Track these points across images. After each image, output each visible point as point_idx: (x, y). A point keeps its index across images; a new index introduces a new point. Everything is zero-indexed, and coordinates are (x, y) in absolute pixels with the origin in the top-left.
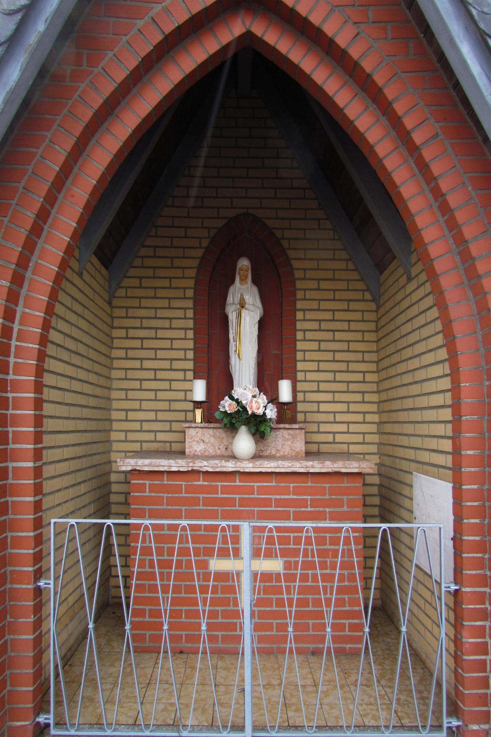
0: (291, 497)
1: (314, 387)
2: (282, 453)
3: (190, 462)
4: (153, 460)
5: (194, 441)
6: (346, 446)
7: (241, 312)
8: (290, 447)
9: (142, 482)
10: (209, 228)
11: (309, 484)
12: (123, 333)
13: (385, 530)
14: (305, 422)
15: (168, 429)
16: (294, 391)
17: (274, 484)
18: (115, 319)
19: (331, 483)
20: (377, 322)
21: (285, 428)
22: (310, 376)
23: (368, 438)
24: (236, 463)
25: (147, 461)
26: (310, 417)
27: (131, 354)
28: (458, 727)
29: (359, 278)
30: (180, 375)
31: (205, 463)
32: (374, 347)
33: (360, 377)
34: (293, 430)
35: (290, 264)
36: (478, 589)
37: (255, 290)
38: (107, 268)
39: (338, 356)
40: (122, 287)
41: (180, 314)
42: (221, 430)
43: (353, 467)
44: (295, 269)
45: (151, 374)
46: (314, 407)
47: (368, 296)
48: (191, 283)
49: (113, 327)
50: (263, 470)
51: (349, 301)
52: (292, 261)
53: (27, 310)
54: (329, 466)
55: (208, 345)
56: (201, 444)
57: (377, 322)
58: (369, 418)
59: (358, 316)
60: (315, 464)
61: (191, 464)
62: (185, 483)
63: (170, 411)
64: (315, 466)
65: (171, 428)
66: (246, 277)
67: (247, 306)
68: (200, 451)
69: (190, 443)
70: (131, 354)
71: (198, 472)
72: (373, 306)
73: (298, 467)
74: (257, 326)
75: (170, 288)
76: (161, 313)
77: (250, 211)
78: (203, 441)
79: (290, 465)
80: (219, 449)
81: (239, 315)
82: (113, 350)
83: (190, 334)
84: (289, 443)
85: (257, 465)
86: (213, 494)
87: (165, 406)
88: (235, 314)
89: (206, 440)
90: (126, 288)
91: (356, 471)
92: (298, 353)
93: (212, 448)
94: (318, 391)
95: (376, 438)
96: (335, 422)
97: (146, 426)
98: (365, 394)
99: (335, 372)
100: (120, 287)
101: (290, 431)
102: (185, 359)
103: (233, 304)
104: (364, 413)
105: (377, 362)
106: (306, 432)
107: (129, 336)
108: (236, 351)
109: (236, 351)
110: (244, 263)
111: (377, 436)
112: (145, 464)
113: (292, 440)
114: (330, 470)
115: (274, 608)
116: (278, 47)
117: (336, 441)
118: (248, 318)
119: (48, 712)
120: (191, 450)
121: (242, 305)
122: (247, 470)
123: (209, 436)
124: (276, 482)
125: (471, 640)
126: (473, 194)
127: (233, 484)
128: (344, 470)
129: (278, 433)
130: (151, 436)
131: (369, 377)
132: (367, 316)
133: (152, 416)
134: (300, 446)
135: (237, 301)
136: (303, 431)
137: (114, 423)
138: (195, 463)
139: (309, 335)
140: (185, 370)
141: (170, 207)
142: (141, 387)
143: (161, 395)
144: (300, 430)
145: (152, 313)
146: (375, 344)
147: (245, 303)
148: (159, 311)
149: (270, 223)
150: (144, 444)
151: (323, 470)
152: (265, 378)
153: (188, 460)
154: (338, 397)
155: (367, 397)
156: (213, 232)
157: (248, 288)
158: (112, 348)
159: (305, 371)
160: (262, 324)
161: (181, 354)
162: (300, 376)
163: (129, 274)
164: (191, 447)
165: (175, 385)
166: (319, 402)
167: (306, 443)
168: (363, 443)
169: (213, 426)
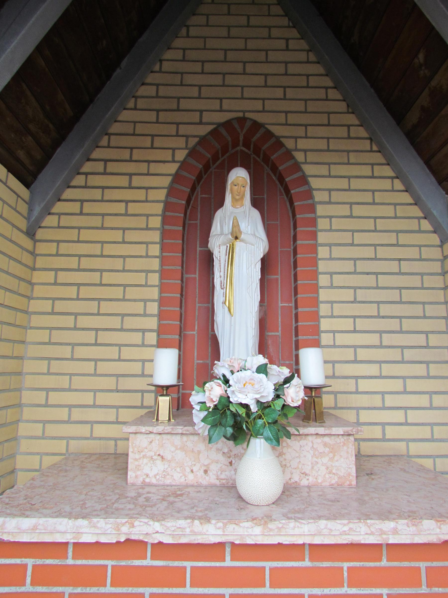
0: (345, 590)
1: (349, 354)
3: (124, 524)
4: (42, 521)
5: (144, 456)
6: (404, 444)
7: (233, 245)
8: (327, 468)
9: (18, 561)
10: (187, 137)
15: (113, 419)
18: (38, 258)
19: (432, 560)
24: (225, 525)
27: (60, 306)
29: (412, 201)
30: (137, 338)
31: (157, 526)
33: (421, 340)
34: (333, 437)
35: (306, 183)
37: (256, 214)
38: (27, 185)
39: (385, 310)
40: (53, 214)
41: (140, 250)
44: (314, 190)
45: (90, 337)
46: (350, 385)
48: (159, 208)
49: (34, 269)
50: (286, 540)
51: (398, 232)
52: (310, 179)
55: (182, 295)
56: (159, 462)
60: (399, 527)
61: (125, 529)
62: (114, 563)
65: (117, 418)
67: (243, 236)
68: (155, 476)
69: (136, 460)
70: (60, 306)
74: (259, 265)
75: (126, 214)
77: (248, 115)
78: (162, 457)
79: (346, 528)
80: (192, 471)
81: (231, 251)
82: (32, 301)
84: (325, 460)
85: (271, 530)
86: (173, 587)
87: (110, 383)
88: (223, 249)
89: (168, 456)
90: (60, 215)
92: (322, 306)
93: (178, 469)
94: (355, 361)
96: (384, 408)
97: (77, 414)
98: (431, 365)
99: (381, 332)
101: (326, 439)
103: (222, 234)
104: (431, 393)
106: (356, 440)
107: (59, 281)
108: (224, 303)
109: (224, 303)
113: (331, 455)
114: (433, 539)
117: (387, 437)
120: (139, 473)
122: (249, 541)
123: (173, 449)
124: (311, 560)
127: (218, 564)
129: (303, 442)
130: (85, 430)
133: (88, 398)
135: (227, 229)
136: (352, 438)
137: (26, 410)
138: (133, 526)
141: (131, 109)
142: (72, 355)
143: (103, 367)
144: (345, 437)
145: (96, 249)
146: (442, 291)
147: (241, 232)
148: (428, 436)
149: (277, 131)
150: (72, 442)
151: (417, 540)
152: (270, 342)
153: (119, 520)
154: (387, 369)
156: (193, 142)
157: (245, 212)
158: (30, 298)
161: (139, 308)
163: (64, 197)
164: (138, 468)
165: (126, 353)
166: (357, 378)
168: (432, 440)
169: (180, 431)
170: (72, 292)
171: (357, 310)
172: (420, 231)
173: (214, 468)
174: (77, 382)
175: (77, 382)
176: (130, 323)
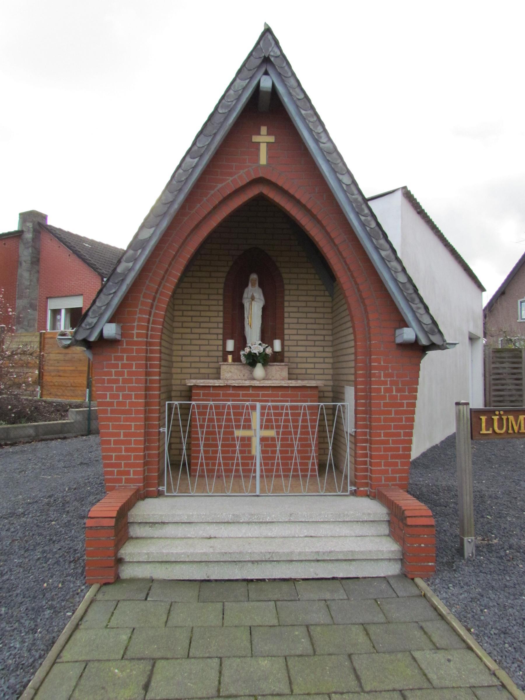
2: (275, 378)
11: (290, 392)
12: (180, 313)
13: (322, 406)
14: (289, 362)
16: (283, 345)
17: (270, 392)
20: (332, 307)
21: (277, 365)
22: (292, 337)
23: (326, 371)
25: (202, 381)
26: (292, 360)
27: (185, 325)
28: (355, 490)
31: (234, 382)
32: (330, 321)
36: (363, 430)
37: (260, 291)
42: (241, 366)
43: (313, 383)
46: (295, 354)
47: (327, 293)
48: (222, 286)
50: (265, 385)
53: (157, 311)
54: (299, 383)
57: (332, 307)
58: (327, 360)
59: (321, 304)
63: (208, 356)
64: (293, 383)
66: (255, 284)
71: (230, 386)
72: (330, 299)
73: (285, 383)
74: (261, 310)
76: (203, 302)
83: (221, 314)
84: (279, 372)
88: (248, 304)
89: (232, 371)
91: (315, 385)
94: (297, 346)
95: (331, 372)
96: (307, 363)
97: (193, 365)
100: (179, 288)
102: (218, 328)
103: (247, 298)
105: (332, 330)
106: (289, 369)
110: (254, 277)
111: (331, 370)
112: (201, 382)
114: (300, 385)
115: (270, 455)
116: (275, 199)
118: (256, 306)
119: (164, 485)
121: (253, 298)
122: (256, 385)
125: (360, 452)
126: (361, 265)
128: (308, 385)
131: (327, 338)
132: (326, 304)
133: (197, 359)
134: (285, 374)
135: (250, 296)
137: (174, 364)
139: (292, 315)
140: (217, 334)
154: (309, 349)
155: (326, 349)
159: (289, 335)
160: (264, 309)
161: (215, 325)
162: (286, 337)
165: (211, 342)
166: (297, 352)
167: (289, 374)
170: (189, 319)
171: (298, 326)
172: (324, 296)
173: (246, 375)
174: (193, 353)
175: (193, 353)
176: (212, 331)
